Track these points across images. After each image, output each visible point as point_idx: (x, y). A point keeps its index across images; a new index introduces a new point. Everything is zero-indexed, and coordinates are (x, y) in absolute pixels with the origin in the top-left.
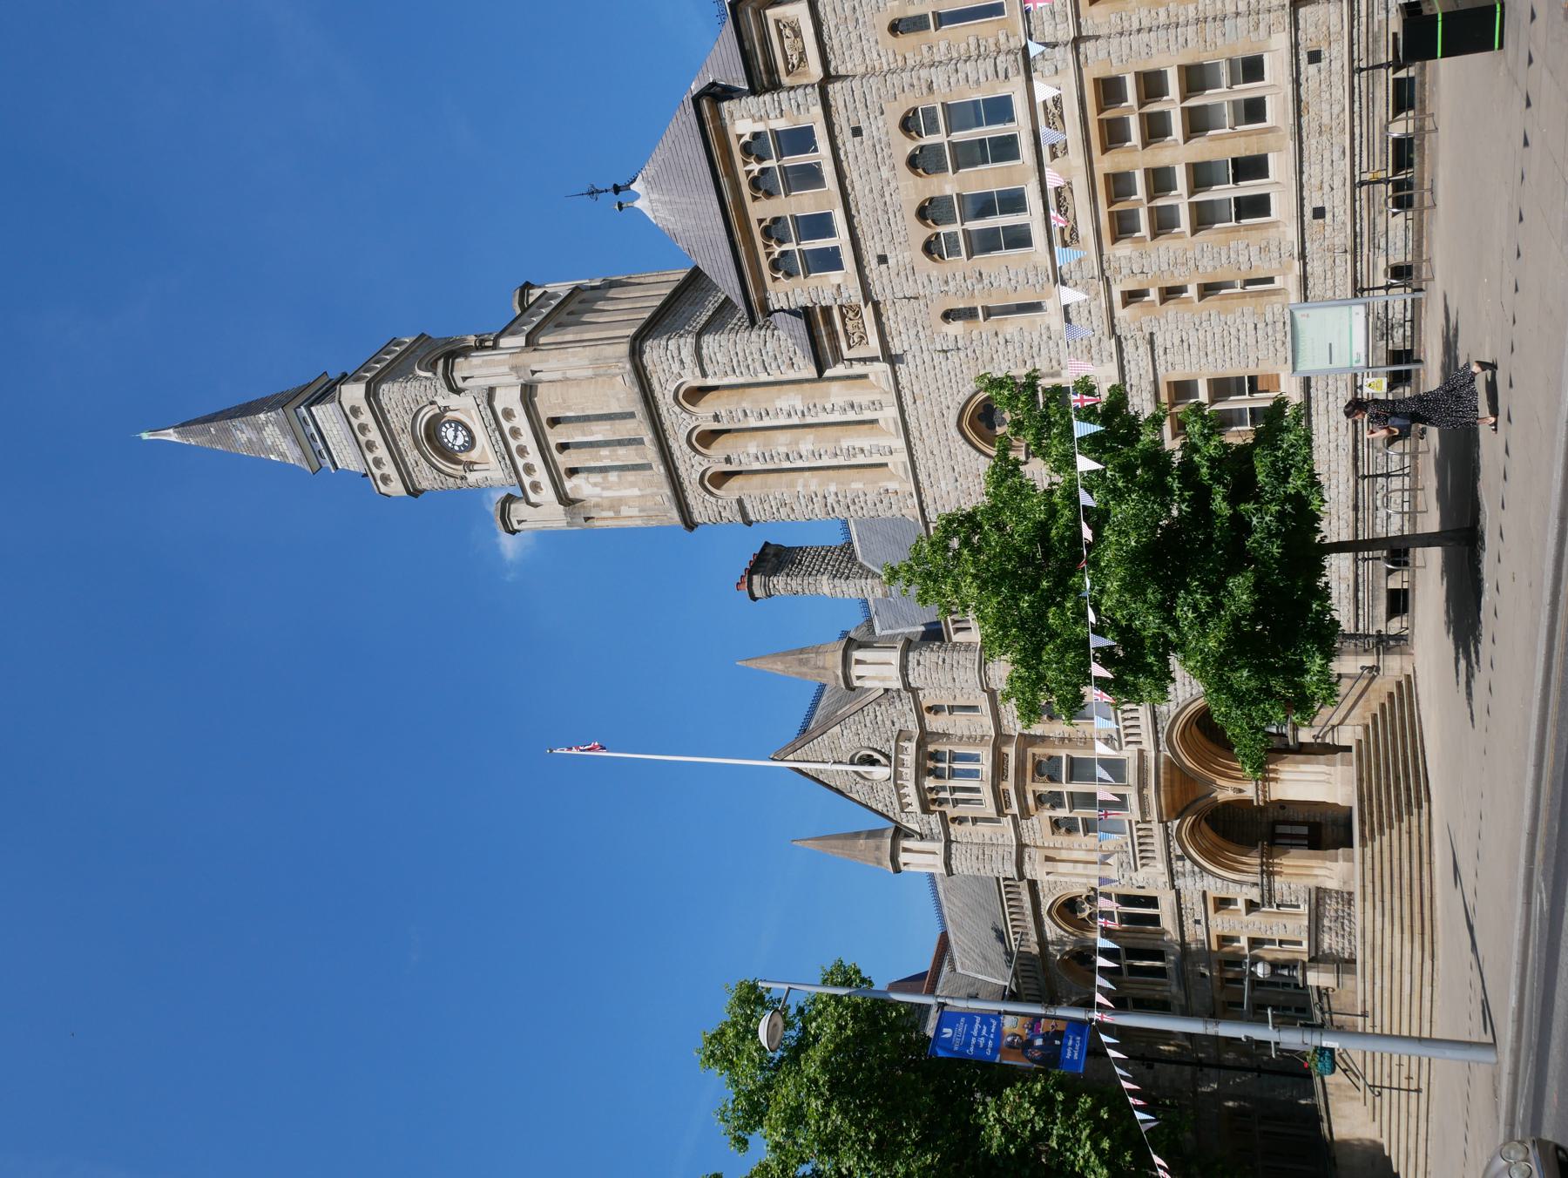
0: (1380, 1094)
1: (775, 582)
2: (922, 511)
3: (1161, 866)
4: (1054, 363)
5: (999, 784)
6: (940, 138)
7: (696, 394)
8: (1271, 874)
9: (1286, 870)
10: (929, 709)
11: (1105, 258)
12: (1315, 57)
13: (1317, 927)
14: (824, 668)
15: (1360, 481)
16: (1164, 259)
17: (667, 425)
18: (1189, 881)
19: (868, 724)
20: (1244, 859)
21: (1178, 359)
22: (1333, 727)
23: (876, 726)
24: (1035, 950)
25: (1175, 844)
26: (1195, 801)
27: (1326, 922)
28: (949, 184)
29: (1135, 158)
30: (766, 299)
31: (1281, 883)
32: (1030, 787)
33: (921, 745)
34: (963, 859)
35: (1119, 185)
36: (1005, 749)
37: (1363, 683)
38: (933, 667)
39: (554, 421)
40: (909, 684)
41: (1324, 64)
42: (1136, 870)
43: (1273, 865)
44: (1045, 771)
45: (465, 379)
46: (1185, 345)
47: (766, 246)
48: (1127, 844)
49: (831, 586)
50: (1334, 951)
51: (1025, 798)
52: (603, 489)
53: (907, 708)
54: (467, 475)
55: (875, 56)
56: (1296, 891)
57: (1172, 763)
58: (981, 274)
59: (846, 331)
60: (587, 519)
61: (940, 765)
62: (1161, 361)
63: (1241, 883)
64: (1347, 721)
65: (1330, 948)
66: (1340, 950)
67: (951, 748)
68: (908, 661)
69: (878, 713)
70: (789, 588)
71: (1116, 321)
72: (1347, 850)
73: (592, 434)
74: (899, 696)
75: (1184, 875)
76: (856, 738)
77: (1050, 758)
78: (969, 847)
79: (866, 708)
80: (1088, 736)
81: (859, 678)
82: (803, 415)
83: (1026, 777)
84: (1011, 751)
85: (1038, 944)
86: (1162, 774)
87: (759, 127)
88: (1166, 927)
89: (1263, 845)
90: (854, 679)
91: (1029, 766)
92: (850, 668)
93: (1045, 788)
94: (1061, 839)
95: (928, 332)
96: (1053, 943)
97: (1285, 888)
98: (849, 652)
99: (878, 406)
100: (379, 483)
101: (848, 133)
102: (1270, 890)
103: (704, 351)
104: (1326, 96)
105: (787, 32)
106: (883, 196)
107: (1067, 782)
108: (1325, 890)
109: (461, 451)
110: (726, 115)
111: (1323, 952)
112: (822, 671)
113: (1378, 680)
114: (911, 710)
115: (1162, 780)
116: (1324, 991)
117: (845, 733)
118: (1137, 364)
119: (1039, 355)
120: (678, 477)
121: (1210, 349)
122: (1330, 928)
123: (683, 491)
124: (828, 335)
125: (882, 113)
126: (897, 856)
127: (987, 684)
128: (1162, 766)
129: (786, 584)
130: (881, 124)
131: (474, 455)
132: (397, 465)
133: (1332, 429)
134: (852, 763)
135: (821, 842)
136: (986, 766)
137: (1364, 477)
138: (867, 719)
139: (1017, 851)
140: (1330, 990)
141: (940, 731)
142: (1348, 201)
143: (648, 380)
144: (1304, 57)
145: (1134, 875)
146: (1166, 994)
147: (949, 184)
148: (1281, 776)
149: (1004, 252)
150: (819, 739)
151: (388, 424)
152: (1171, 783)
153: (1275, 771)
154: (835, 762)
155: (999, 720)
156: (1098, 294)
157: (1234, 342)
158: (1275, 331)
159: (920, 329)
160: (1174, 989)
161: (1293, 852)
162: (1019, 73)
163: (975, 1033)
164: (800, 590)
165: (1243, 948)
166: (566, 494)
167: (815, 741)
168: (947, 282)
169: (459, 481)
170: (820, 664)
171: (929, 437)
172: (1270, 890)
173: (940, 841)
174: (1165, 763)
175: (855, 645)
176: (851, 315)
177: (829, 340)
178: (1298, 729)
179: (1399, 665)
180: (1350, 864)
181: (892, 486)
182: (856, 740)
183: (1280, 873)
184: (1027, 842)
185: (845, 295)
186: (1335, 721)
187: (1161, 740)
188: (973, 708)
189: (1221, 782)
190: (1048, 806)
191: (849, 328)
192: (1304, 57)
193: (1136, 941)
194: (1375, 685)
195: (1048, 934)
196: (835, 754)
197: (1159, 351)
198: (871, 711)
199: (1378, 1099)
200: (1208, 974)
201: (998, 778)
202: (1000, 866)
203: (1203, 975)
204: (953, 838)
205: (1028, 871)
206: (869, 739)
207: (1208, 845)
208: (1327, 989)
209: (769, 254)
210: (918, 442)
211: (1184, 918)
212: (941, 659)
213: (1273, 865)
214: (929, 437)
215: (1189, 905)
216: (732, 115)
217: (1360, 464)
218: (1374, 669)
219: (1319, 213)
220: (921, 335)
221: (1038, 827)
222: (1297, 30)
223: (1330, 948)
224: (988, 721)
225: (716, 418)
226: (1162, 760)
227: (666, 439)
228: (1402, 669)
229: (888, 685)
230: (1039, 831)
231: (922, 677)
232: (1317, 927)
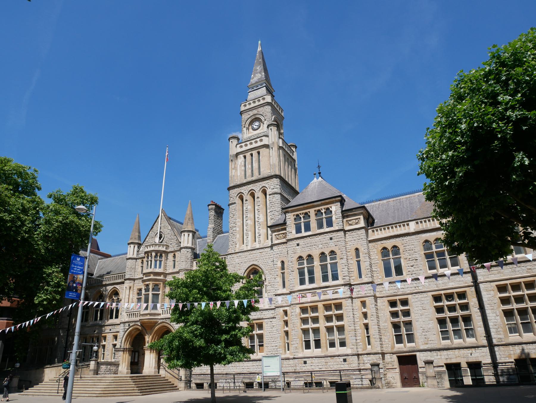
2: (230, 254)
4: (269, 291)
5: (152, 274)
6: (329, 261)
7: (265, 192)
9: (152, 354)
10: (175, 254)
11: (296, 305)
12: (345, 360)
14: (187, 225)
16: (295, 321)
17: (257, 184)
19: (171, 237)
20: (128, 343)
21: (269, 325)
22: (165, 368)
24: (104, 283)
25: (133, 324)
26: (145, 330)
27: (109, 367)
28: (317, 263)
29: (321, 313)
30: (289, 213)
32: (151, 283)
33: (164, 252)
35: (315, 309)
36: (162, 276)
37: (177, 376)
38: (187, 256)
39: (259, 153)
41: (343, 363)
42: (126, 313)
43: (126, 352)
45: (271, 129)
46: (273, 327)
47: (303, 213)
51: (148, 281)
52: (240, 165)
53: (175, 248)
54: (245, 128)
55: (350, 244)
57: (157, 323)
58: (293, 271)
59: (280, 234)
60: (232, 160)
61: (158, 257)
62: (268, 320)
64: (166, 372)
67: (163, 261)
68: (188, 249)
71: (279, 308)
73: (255, 163)
75: (124, 326)
76: (167, 233)
81: (184, 235)
82: (258, 222)
84: (162, 277)
87: (333, 213)
88: (109, 321)
90: (184, 233)
91: (157, 283)
93: (151, 287)
94: (136, 291)
95: (278, 257)
96: (106, 288)
99: (259, 242)
100: (244, 104)
101: (331, 236)
102: (119, 351)
103: (276, 195)
104: (335, 363)
105: (357, 221)
106: (314, 245)
109: (252, 126)
110: (337, 204)
115: (152, 320)
118: (268, 314)
119: (271, 287)
120: (242, 186)
121: (271, 334)
122: (107, 368)
123: (238, 187)
124: (279, 229)
125: (336, 246)
126: (133, 244)
128: (156, 320)
130: (333, 245)
131: (251, 130)
132: (249, 109)
133: (248, 367)
134: (160, 232)
136: (157, 270)
137: (234, 376)
139: (133, 279)
142: (308, 370)
143: (269, 179)
144: (345, 357)
145: (125, 312)
147: (317, 263)
148: (152, 354)
149: (299, 278)
151: (260, 107)
152: (151, 323)
153: (153, 352)
154: (160, 227)
156: (287, 303)
157: (273, 340)
158: (275, 351)
159: (279, 255)
160: (91, 323)
162: (344, 282)
163: (78, 267)
164: (210, 219)
165: (102, 343)
166: (239, 155)
168: (291, 262)
169: (244, 125)
170: (189, 224)
171: (250, 256)
172: (119, 351)
173: (137, 256)
174: (157, 321)
176: (284, 236)
177: (277, 230)
181: (238, 246)
183: (124, 353)
184: (135, 282)
185: (289, 234)
189: (151, 337)
190: (146, 288)
191: (280, 235)
192: (345, 357)
195: (108, 287)
197: (271, 320)
198: (175, 238)
200: (95, 333)
202: (129, 274)
203: (95, 331)
204: (137, 260)
208: (89, 367)
209: (300, 214)
210: (249, 253)
213: (126, 352)
214: (250, 256)
216: (336, 205)
217: (238, 375)
218: (181, 380)
219: (305, 363)
220: (278, 255)
222: (352, 356)
223: (101, 368)
225: (258, 198)
226: (158, 320)
227: (253, 184)
228: (181, 387)
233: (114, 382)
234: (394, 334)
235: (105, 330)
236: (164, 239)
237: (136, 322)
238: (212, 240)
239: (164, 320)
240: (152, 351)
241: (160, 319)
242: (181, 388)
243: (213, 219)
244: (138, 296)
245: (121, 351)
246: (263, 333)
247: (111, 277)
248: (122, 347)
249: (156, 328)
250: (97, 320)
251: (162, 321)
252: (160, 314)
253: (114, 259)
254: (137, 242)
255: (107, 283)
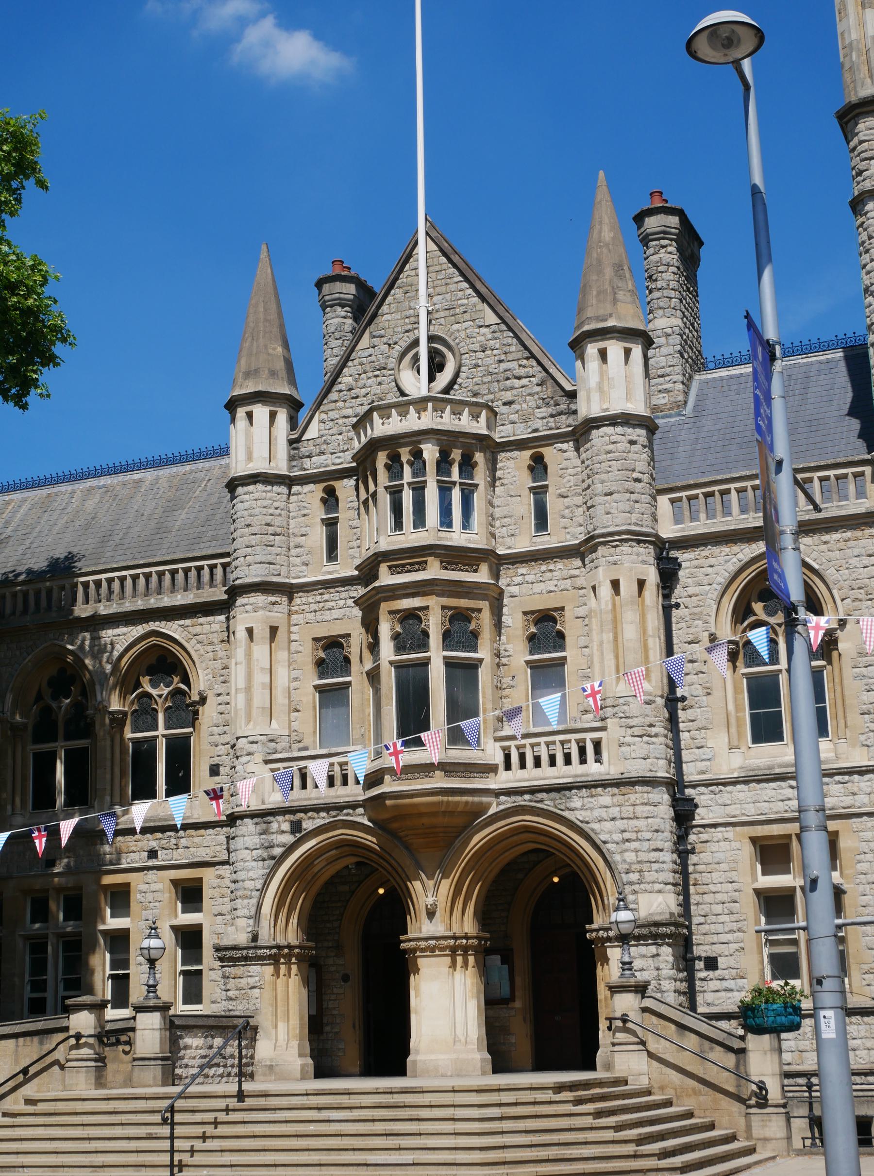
0: (165, 1121)
1: (670, 249)
3: (275, 799)
5: (436, 556)
8: (274, 960)
9: (282, 980)
13: (211, 1027)
14: (615, 301)
15: (802, 1081)
18: (254, 840)
19: (503, 366)
20: (294, 921)
22: (643, 1043)
23: (501, 377)
24: (82, 610)
25: (322, 819)
26: (408, 847)
27: (218, 1041)
31: (261, 976)
32: (434, 602)
33: (484, 442)
34: (265, 503)
36: (484, 568)
37: (728, 1082)
38: (628, 464)
40: (598, 427)
42: (267, 762)
43: (289, 963)
44: (456, 627)
48: (306, 749)
49: (669, 331)
50: (182, 1052)
53: (538, 424)
56: (248, 998)
57: (478, 814)
61: (455, 470)
63: (257, 916)
64: (655, 1063)
65: (186, 1047)
66: (185, 1061)
67: (481, 488)
68: (634, 426)
69: (525, 381)
70: (661, 269)
72: (311, 1070)
74: (561, 413)
75: (264, 832)
76: (476, 347)
77: (475, 635)
78: (283, 512)
79: (534, 363)
80: (506, 692)
81: (250, 415)
83: (448, 597)
84: (482, 576)
85: (93, 616)
86: (465, 799)
89: (311, 948)
90: (602, 345)
91: (464, 603)
92: (618, 339)
93: (435, 624)
94: (307, 653)
96: (95, 639)
97: (251, 981)
98: (640, 340)
102: (246, 958)
107: (445, 657)
108: (254, 1039)
111: (181, 1037)
112: (610, 298)
113: (736, 1107)
114: (536, 431)
115: (457, 799)
116: (123, 1038)
117: (484, 330)
122: (211, 1047)
127: (604, 543)
128: (476, 799)
129: (668, 265)
134: (431, 338)
135: (270, 288)
136: (457, 537)
138: (514, 365)
140: (127, 1048)
141: (499, 474)
145: (259, 758)
146: (9, 807)
148: (459, 974)
150: (470, 291)
152: (450, 812)
153: (466, 964)
154: (429, 313)
155: (526, 562)
161: (305, 992)
164: (659, 284)
165: (104, 922)
167: (465, 285)
170: (620, 295)
172: (246, 958)
173: (291, 468)
174: (481, 803)
175: (293, 413)
178: (636, 992)
179: (772, 1136)
180: (299, 1076)
182: (472, 347)
183: (277, 973)
184: (297, 601)
186: (653, 1045)
187: (518, 798)
188: (541, 521)
189: (446, 886)
190: (398, 629)
193: (108, 764)
194: (726, 1102)
196: (442, 314)
198: (530, 371)
199: (157, 1118)
201: (445, 555)
202: (258, 558)
204: (295, 489)
205: (252, 600)
206: (477, 366)
207: (316, 869)
208: (129, 1043)
211: (159, 835)
212: (640, 476)
213: (289, 963)
215: (183, 842)
218: (762, 1099)
221: (328, 618)
223: (186, 1047)
224: (523, 543)
226: (485, 799)
228: (766, 1140)
229: (581, 396)
230: (320, 618)
231: (611, 447)
232: (211, 1027)
233: (501, 1119)
234: (180, 968)
235: (119, 853)
236: (457, 375)
237: (340, 807)
238: (681, 398)
239: (521, 801)
240: (459, 959)
241: (498, 793)
242: (770, 1145)
243: (673, 284)
244: (321, 676)
245: (442, 949)
246: (128, 929)
247: (122, 579)
248: (265, 938)
249: (478, 839)
250: (53, 805)
251: (507, 802)
252: (491, 769)
253: (49, 496)
254: (287, 391)
255: (104, 609)
